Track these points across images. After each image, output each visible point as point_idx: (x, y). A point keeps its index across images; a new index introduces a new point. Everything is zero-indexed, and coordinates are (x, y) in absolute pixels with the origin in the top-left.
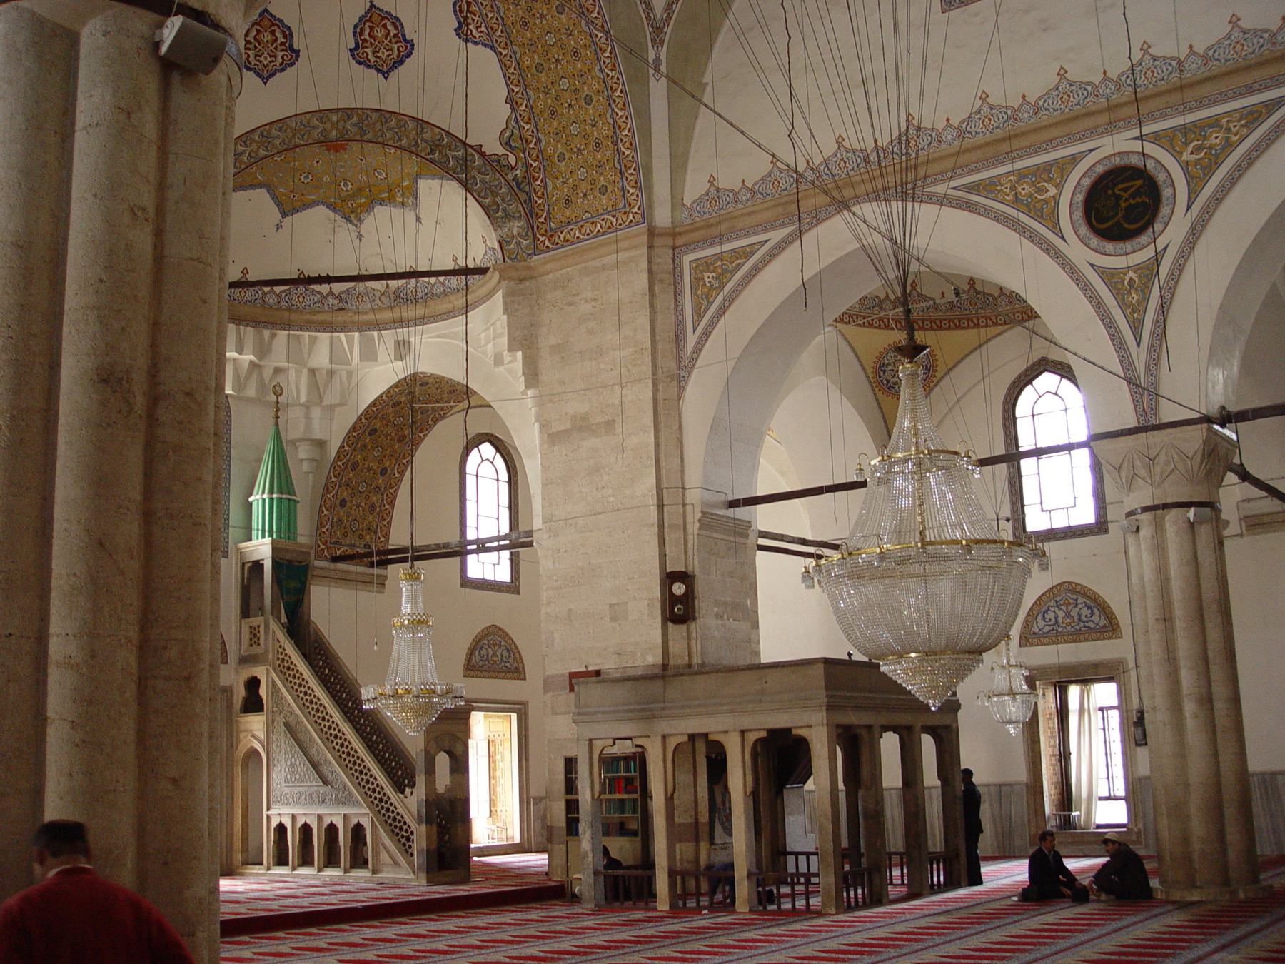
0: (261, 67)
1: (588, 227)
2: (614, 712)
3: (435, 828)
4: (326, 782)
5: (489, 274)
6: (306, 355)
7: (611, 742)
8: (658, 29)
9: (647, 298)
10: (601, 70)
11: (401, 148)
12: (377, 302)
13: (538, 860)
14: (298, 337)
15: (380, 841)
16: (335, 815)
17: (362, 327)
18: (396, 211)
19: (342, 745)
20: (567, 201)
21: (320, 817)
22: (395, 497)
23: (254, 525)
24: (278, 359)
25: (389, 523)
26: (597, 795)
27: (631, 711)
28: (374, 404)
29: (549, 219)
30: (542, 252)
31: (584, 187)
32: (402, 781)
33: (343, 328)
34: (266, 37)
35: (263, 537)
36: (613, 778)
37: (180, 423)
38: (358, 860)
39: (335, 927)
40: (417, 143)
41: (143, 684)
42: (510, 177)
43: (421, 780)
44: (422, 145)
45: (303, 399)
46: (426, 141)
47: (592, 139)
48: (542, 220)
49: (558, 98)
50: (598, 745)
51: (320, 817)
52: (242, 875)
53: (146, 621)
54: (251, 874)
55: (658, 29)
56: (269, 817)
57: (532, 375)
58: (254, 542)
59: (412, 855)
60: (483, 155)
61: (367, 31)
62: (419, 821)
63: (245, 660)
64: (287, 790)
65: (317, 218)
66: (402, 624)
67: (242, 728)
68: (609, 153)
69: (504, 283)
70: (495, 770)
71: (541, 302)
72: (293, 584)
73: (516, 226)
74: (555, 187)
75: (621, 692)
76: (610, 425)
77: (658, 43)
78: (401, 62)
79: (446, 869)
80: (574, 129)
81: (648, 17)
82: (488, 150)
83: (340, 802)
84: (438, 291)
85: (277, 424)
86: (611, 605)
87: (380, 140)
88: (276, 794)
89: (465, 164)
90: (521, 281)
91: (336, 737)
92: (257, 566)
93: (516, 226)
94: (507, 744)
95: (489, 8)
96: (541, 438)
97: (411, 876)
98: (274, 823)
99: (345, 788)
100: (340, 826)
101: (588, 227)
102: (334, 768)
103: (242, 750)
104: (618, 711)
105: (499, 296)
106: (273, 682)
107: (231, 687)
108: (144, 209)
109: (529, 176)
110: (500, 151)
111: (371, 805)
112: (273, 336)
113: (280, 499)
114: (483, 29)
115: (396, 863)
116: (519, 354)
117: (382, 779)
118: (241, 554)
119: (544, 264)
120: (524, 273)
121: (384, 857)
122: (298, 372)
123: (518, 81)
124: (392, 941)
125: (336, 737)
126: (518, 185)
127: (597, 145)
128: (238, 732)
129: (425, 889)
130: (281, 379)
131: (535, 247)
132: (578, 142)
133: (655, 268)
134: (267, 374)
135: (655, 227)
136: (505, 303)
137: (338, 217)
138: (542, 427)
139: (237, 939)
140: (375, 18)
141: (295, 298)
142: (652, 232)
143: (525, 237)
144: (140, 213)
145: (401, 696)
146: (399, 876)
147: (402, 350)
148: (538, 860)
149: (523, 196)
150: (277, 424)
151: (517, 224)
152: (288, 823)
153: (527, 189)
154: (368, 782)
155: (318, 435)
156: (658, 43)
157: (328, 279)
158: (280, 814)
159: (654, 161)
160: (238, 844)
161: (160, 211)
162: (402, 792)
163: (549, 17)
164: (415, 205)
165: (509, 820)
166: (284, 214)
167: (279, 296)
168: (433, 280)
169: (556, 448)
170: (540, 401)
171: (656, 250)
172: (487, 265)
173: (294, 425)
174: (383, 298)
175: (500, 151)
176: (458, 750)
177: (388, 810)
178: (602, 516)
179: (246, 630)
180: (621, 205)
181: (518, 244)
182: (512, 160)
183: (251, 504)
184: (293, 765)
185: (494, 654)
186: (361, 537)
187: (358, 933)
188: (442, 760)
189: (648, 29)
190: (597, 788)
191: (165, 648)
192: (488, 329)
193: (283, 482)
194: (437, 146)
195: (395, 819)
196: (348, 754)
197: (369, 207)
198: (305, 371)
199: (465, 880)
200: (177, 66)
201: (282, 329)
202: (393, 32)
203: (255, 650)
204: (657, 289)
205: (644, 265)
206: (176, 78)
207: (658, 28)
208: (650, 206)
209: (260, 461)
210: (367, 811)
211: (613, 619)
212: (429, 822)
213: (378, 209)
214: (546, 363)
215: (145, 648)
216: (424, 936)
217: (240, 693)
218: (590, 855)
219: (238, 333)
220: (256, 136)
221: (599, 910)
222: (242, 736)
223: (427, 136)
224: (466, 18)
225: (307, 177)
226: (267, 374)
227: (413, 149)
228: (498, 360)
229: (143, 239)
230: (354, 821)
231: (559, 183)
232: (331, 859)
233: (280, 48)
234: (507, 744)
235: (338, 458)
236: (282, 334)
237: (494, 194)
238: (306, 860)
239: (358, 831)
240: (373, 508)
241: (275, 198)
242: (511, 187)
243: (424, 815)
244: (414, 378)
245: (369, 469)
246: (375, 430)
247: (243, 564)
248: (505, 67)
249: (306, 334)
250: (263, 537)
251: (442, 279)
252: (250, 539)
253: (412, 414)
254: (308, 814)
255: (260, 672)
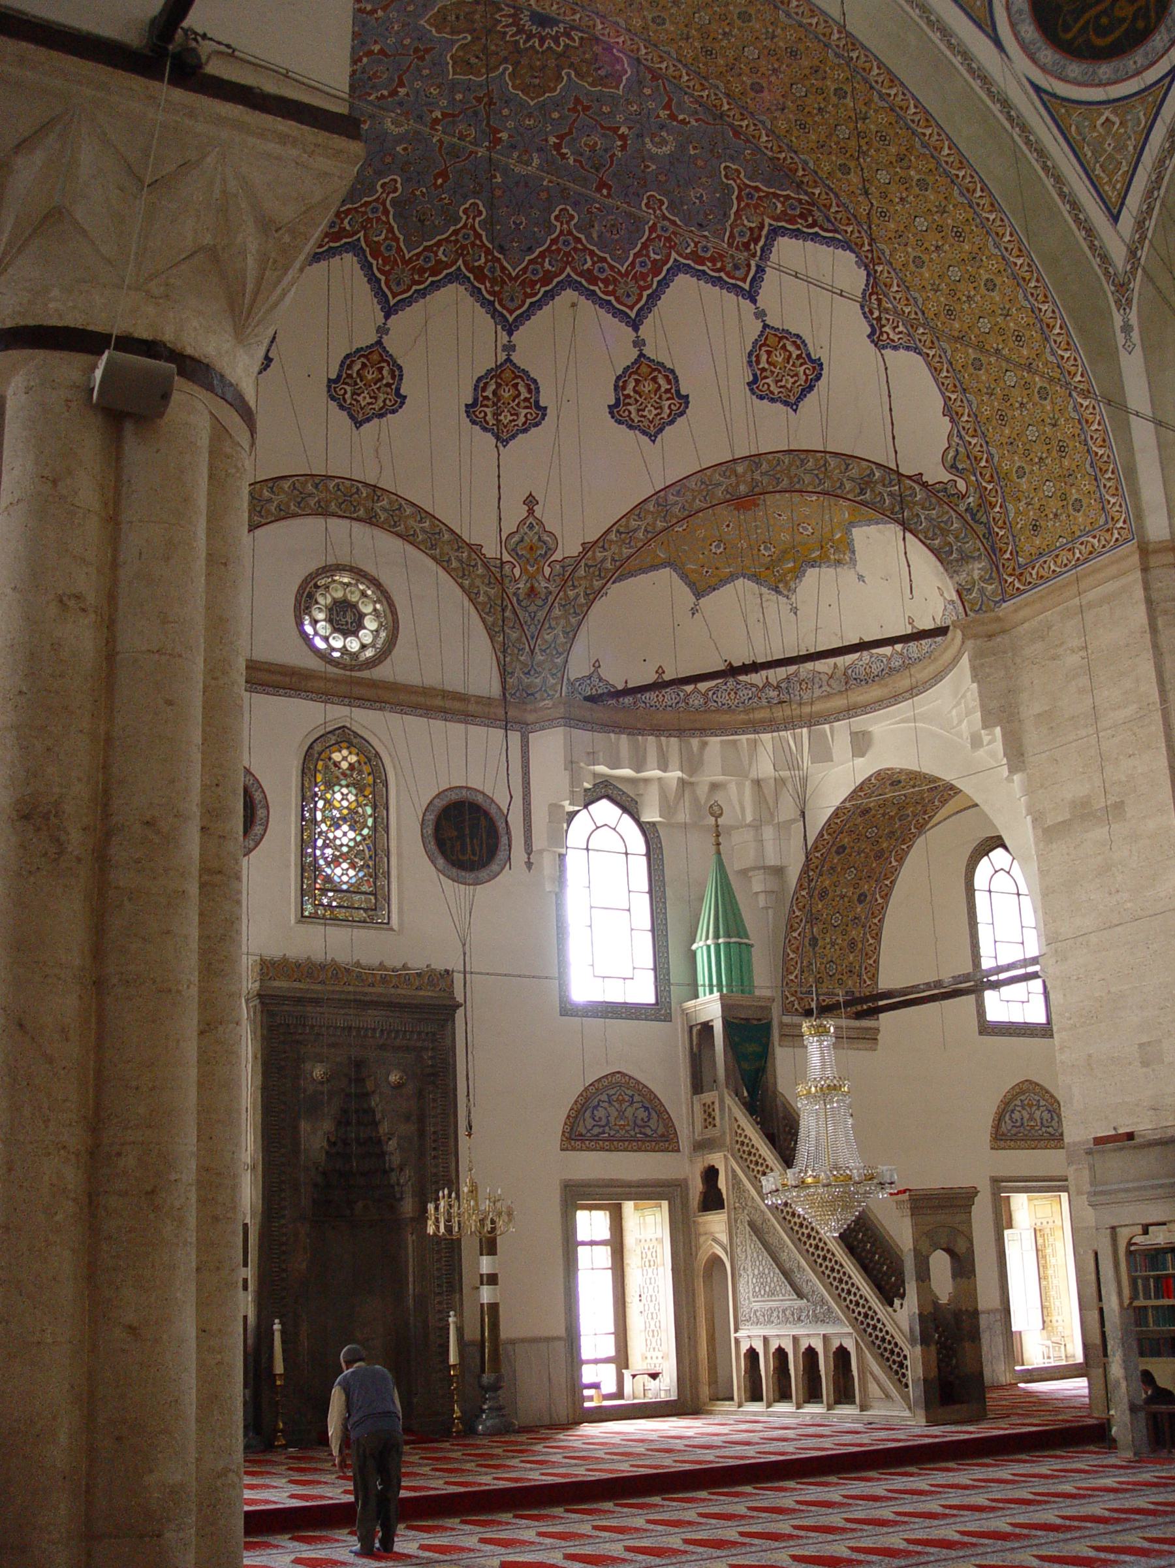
0: (646, 423)
1: (1064, 556)
2: (1153, 1187)
3: (933, 1348)
4: (800, 1295)
5: (950, 634)
6: (747, 767)
7: (1139, 1230)
8: (1122, 287)
9: (1148, 636)
10: (1053, 353)
11: (825, 493)
12: (825, 688)
13: (1078, 1386)
14: (735, 741)
15: (868, 1369)
16: (813, 1336)
17: (812, 721)
18: (827, 573)
19: (817, 1247)
20: (1035, 527)
21: (825, 1338)
22: (881, 929)
23: (700, 982)
24: (712, 772)
25: (877, 961)
26: (1126, 1302)
27: (1161, 1186)
28: (836, 814)
29: (1016, 553)
30: (1013, 597)
31: (1054, 505)
32: (890, 1292)
33: (790, 724)
34: (648, 387)
35: (711, 992)
36: (1157, 1278)
37: (138, 861)
38: (844, 1395)
39: (943, 1465)
40: (842, 484)
41: (92, 1202)
42: (962, 508)
43: (911, 1288)
44: (848, 486)
45: (749, 818)
46: (853, 480)
47: (1054, 443)
48: (1007, 556)
49: (1006, 398)
50: (1124, 1234)
51: (796, 1339)
52: (710, 1413)
53: (96, 1121)
54: (720, 1413)
55: (1122, 287)
56: (737, 1341)
57: (1016, 755)
58: (701, 999)
59: (907, 1386)
60: (925, 485)
61: (764, 357)
62: (913, 1342)
63: (702, 1146)
64: (756, 1306)
65: (737, 597)
66: (809, 1092)
67: (702, 1230)
68: (1077, 456)
69: (970, 643)
70: (1045, 1267)
71: (1018, 660)
72: (751, 1048)
73: (977, 569)
74: (1018, 512)
75: (1147, 1162)
76: (1119, 806)
77: (1124, 303)
78: (811, 388)
79: (954, 1402)
80: (1032, 433)
81: (1107, 273)
82: (929, 478)
83: (818, 1320)
84: (896, 663)
85: (719, 853)
86: (1141, 1045)
87: (797, 487)
88: (744, 1310)
89: (903, 501)
90: (990, 637)
91: (809, 1236)
92: (707, 1028)
93: (977, 569)
94: (1059, 1233)
95: (903, 302)
96: (1036, 836)
97: (907, 1414)
98: (744, 1348)
99: (823, 1302)
100: (760, 1350)
101: (1064, 556)
102: (810, 1278)
103: (703, 1257)
104: (1144, 1188)
105: (965, 660)
106: (733, 1171)
107: (686, 1180)
108: (78, 597)
109: (985, 503)
110: (946, 477)
111: (854, 1322)
112: (705, 744)
113: (727, 944)
114: (901, 328)
115: (888, 1396)
116: (998, 730)
117: (865, 1289)
118: (685, 1014)
119: (1016, 611)
120: (995, 627)
121: (873, 1388)
122: (740, 786)
123: (954, 387)
124: (966, 1487)
125: (809, 1236)
126: (973, 516)
127: (1061, 449)
128: (698, 1235)
129: (918, 1431)
130: (719, 797)
131: (1004, 592)
132: (1039, 450)
133: (1155, 596)
134: (702, 791)
135: (1148, 543)
136: (973, 668)
137: (764, 590)
138: (1034, 821)
139: (776, 1485)
140: (772, 341)
141: (725, 694)
142: (1144, 551)
143: (989, 580)
144: (72, 603)
145: (808, 1187)
146: (890, 1412)
147: (861, 743)
148: (1078, 1386)
149: (981, 530)
150: (719, 853)
151: (977, 565)
152: (759, 1347)
153: (984, 519)
154: (849, 1292)
155: (772, 860)
156: (1124, 303)
157: (755, 667)
158: (749, 1336)
159: (1138, 456)
160: (704, 1375)
161: (112, 597)
162: (891, 1304)
163: (978, 298)
164: (853, 562)
165: (1067, 1333)
166: (699, 595)
167: (705, 695)
168: (887, 650)
169: (1054, 846)
170: (1029, 791)
171: (1154, 573)
172: (948, 622)
173: (742, 851)
174: (832, 682)
175: (946, 477)
176: (961, 1247)
177: (875, 1328)
178: (1119, 929)
179: (697, 1107)
180: (1102, 521)
181: (982, 591)
182: (961, 485)
183: (694, 954)
184: (761, 1275)
185: (1031, 1118)
186: (841, 982)
187: (791, 1494)
188: (940, 1263)
189: (1109, 288)
190: (1126, 1292)
191: (119, 1154)
192: (958, 704)
193: (731, 923)
194: (867, 483)
195: (883, 1340)
196: (825, 1258)
197: (798, 573)
198: (748, 783)
199: (979, 1417)
200: (129, 415)
201: (712, 735)
202: (796, 353)
203: (711, 1133)
204: (1160, 622)
205: (1139, 593)
206: (129, 427)
207: (1122, 286)
208: (1139, 517)
209: (702, 899)
210: (850, 1330)
211: (1145, 1064)
212: (925, 1340)
213: (811, 574)
214: (1032, 737)
215: (96, 1158)
216: (966, 1487)
217: (697, 1186)
218: (1124, 1384)
219: (660, 747)
220: (651, 506)
221: (1139, 1461)
222: (702, 1239)
223: (854, 472)
224: (879, 319)
225: (718, 547)
226: (702, 791)
227: (839, 492)
228: (976, 742)
229: (81, 636)
230: (836, 1344)
231: (1022, 506)
232: (812, 1394)
233: (665, 396)
234: (1059, 1233)
235: (800, 886)
236: (714, 741)
237: (945, 532)
238: (783, 1395)
239: (842, 1355)
240: (853, 944)
241: (684, 577)
242: (962, 520)
243: (918, 1333)
244: (888, 779)
245: (842, 897)
246: (844, 848)
247: (691, 1028)
248: (935, 371)
249: (744, 737)
250: (711, 992)
251: (898, 647)
252: (696, 997)
253: (891, 821)
254: (782, 1335)
255: (716, 1159)
